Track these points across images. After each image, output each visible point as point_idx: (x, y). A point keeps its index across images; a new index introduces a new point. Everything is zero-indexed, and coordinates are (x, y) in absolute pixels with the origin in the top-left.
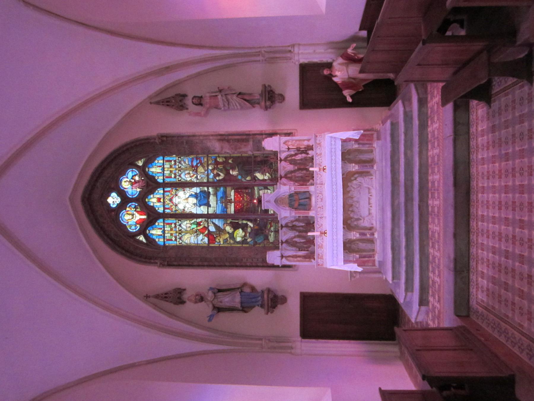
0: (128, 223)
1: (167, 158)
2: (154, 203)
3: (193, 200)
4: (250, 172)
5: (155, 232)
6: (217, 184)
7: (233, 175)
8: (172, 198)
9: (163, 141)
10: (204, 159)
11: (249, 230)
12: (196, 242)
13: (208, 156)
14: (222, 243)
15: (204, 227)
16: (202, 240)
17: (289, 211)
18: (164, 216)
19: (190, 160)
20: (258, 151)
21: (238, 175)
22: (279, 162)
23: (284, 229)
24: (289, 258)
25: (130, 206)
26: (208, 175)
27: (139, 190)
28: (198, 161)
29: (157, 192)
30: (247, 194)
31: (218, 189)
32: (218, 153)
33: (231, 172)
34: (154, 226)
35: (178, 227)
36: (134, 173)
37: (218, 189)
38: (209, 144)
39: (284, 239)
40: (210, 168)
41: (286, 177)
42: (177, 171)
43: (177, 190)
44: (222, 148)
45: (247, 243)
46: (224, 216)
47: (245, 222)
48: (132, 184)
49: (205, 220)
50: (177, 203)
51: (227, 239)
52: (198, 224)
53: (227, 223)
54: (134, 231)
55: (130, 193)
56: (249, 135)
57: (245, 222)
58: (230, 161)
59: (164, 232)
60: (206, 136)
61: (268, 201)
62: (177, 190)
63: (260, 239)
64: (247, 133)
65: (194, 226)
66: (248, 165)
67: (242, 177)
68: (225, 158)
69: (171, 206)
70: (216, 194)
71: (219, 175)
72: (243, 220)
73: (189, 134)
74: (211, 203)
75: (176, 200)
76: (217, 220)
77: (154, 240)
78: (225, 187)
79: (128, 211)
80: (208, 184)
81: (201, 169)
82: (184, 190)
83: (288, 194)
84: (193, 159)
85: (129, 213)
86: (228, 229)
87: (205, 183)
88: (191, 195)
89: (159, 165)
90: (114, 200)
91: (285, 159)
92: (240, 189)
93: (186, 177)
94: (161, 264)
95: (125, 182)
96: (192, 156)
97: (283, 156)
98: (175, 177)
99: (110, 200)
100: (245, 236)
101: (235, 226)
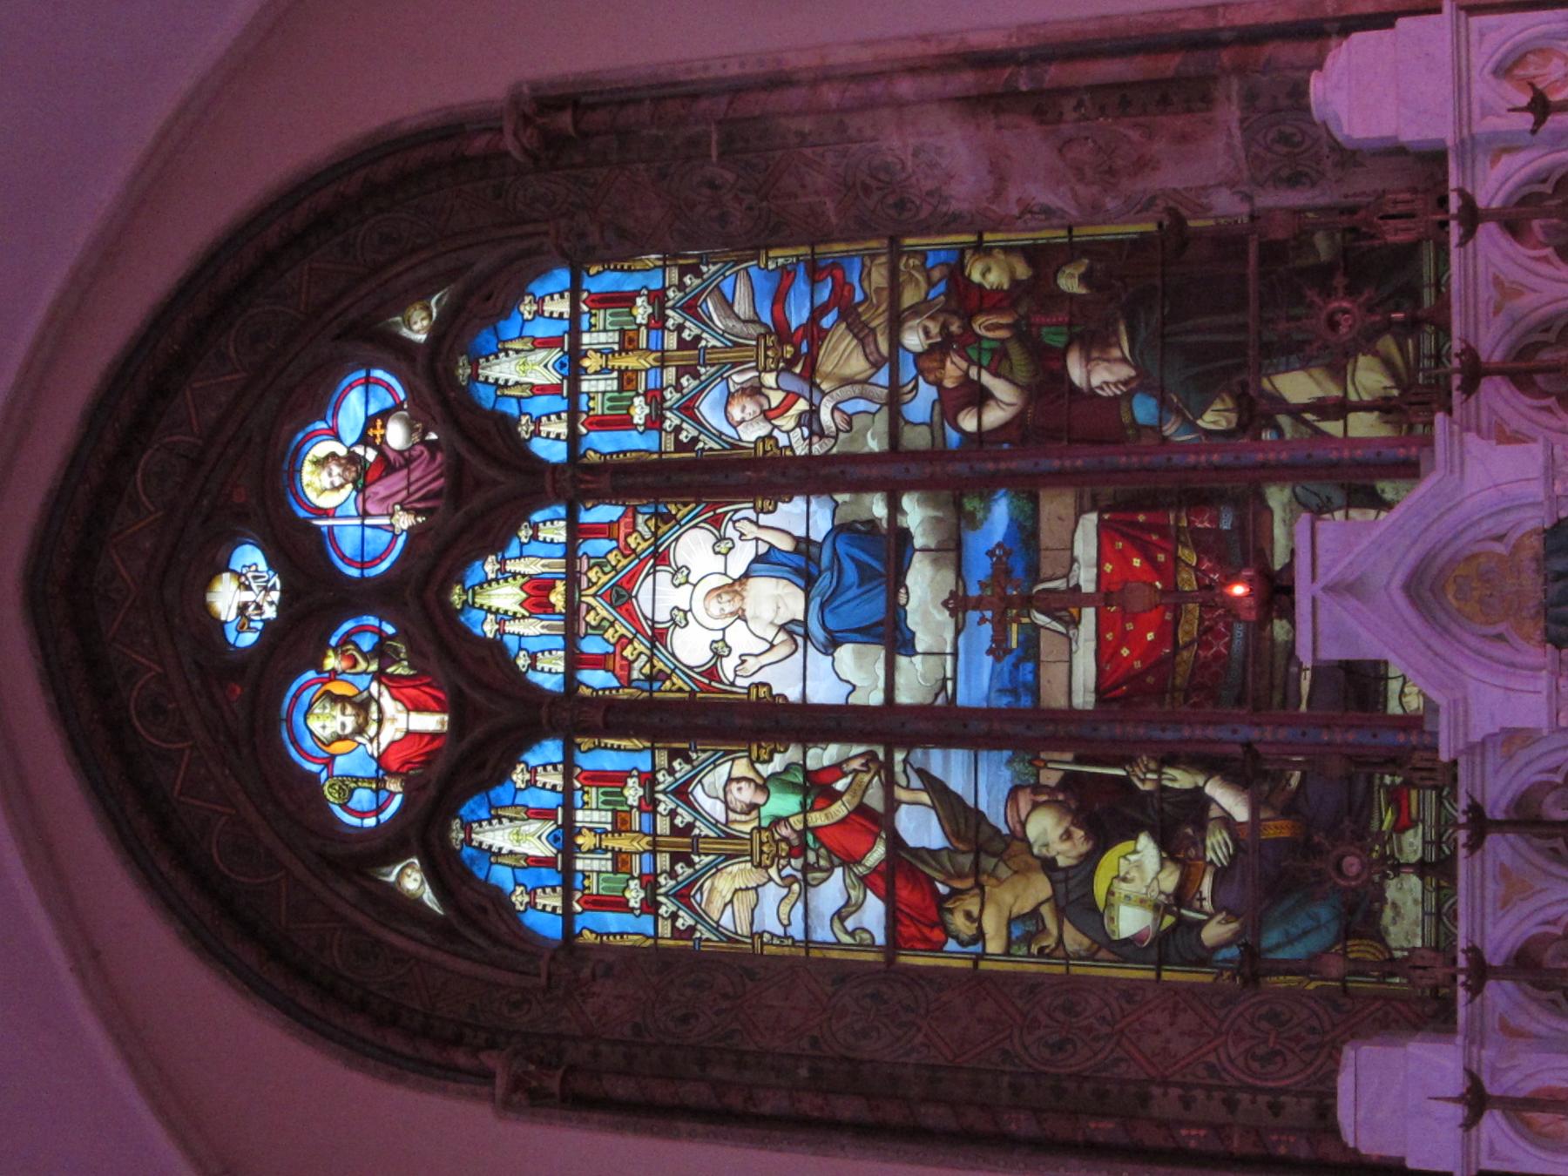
0: (329, 761)
1: (602, 281)
2: (502, 617)
3: (777, 599)
5: (511, 839)
6: (961, 468)
7: (1091, 395)
8: (633, 576)
9: (553, 142)
10: (865, 275)
11: (1217, 846)
12: (797, 931)
13: (894, 241)
14: (994, 946)
15: (862, 810)
16: (841, 910)
17: (1543, 682)
18: (576, 717)
19: (765, 287)
20: (1294, 181)
22: (1455, 231)
23: (1499, 847)
25: (346, 639)
26: (894, 401)
27: (404, 521)
28: (824, 294)
29: (524, 534)
30: (1200, 543)
31: (970, 504)
32: (979, 223)
34: (501, 793)
35: (666, 804)
37: (970, 504)
38: (896, 144)
39: (1501, 934)
40: (913, 340)
41: (1522, 371)
43: (668, 518)
45: (1202, 957)
47: (1181, 779)
48: (363, 476)
49: (870, 757)
50: (662, 616)
51: (1035, 913)
52: (817, 788)
53: (1037, 788)
54: (370, 822)
56: (1204, 42)
57: (1181, 779)
58: (1069, 282)
59: (567, 837)
60: (868, 84)
62: (668, 518)
63: (1299, 936)
65: (784, 804)
66: (1208, 297)
67: (1163, 403)
68: (1032, 254)
69: (623, 641)
70: (951, 550)
71: (980, 397)
72: (1171, 760)
74: (913, 621)
75: (658, 596)
77: (499, 898)
78: (1028, 489)
80: (893, 471)
81: (843, 356)
82: (716, 522)
84: (785, 277)
85: (337, 688)
86: (1045, 829)
87: (872, 458)
89: (541, 330)
90: (243, 595)
93: (734, 420)
94: (517, 1084)
95: (321, 463)
96: (780, 256)
97: (1493, 183)
98: (655, 422)
99: (225, 598)
100: (1182, 895)
101: (1105, 816)
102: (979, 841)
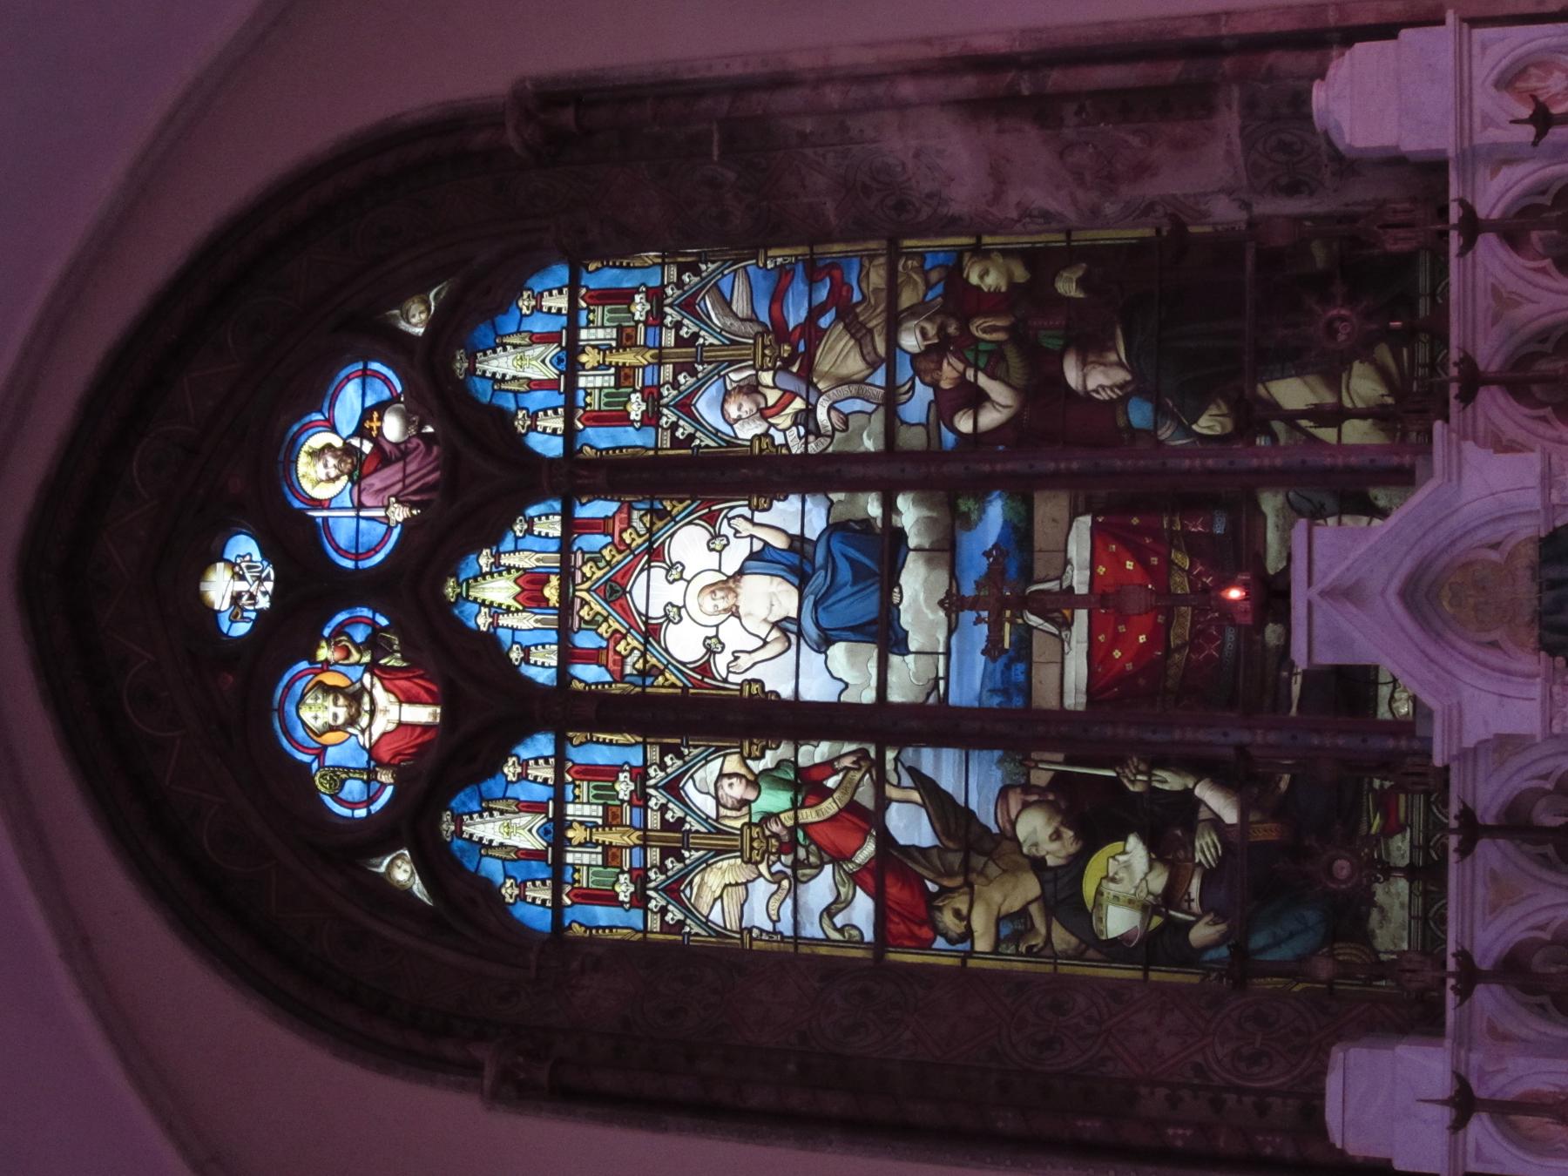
0: (321, 752)
1: (601, 277)
2: (496, 610)
3: (770, 597)
4: (1228, 374)
7: (1086, 398)
8: (627, 572)
10: (863, 276)
11: (1206, 848)
14: (983, 944)
16: (833, 906)
18: (568, 711)
19: (763, 286)
21: (1127, 392)
22: (1455, 241)
23: (1489, 852)
24: (1527, 1121)
25: (340, 630)
26: (891, 401)
27: (399, 513)
28: (822, 294)
30: (1193, 546)
31: (965, 505)
32: (977, 226)
33: (1072, 376)
34: (493, 786)
35: (657, 799)
36: (378, 393)
37: (965, 505)
40: (910, 341)
41: (1519, 381)
42: (667, 371)
43: (662, 514)
44: (999, 179)
45: (1189, 957)
46: (1003, 726)
47: (1171, 781)
49: (862, 755)
50: (656, 611)
51: (1023, 913)
52: (807, 785)
53: (1027, 788)
54: (361, 813)
55: (343, 532)
56: (1205, 49)
57: (1171, 781)
58: (1067, 286)
59: (557, 831)
60: (871, 85)
61: (1346, 593)
62: (662, 514)
63: (1283, 941)
64: (1192, 32)
65: (774, 800)
66: (1208, 307)
68: (1029, 257)
69: (617, 636)
70: (945, 551)
73: (737, 69)
74: (906, 620)
75: (652, 592)
76: (950, 756)
77: (490, 890)
78: (1022, 492)
79: (327, 665)
80: (889, 471)
81: (840, 355)
83: (1530, 528)
85: (330, 679)
86: (1034, 827)
87: (866, 457)
88: (760, 558)
89: (539, 325)
90: (235, 585)
91: (1513, 232)
92: (1132, 508)
93: (730, 417)
95: (316, 454)
96: (778, 256)
97: (1493, 193)
98: (651, 419)
100: (1171, 896)
101: (1095, 817)
102: (968, 841)
